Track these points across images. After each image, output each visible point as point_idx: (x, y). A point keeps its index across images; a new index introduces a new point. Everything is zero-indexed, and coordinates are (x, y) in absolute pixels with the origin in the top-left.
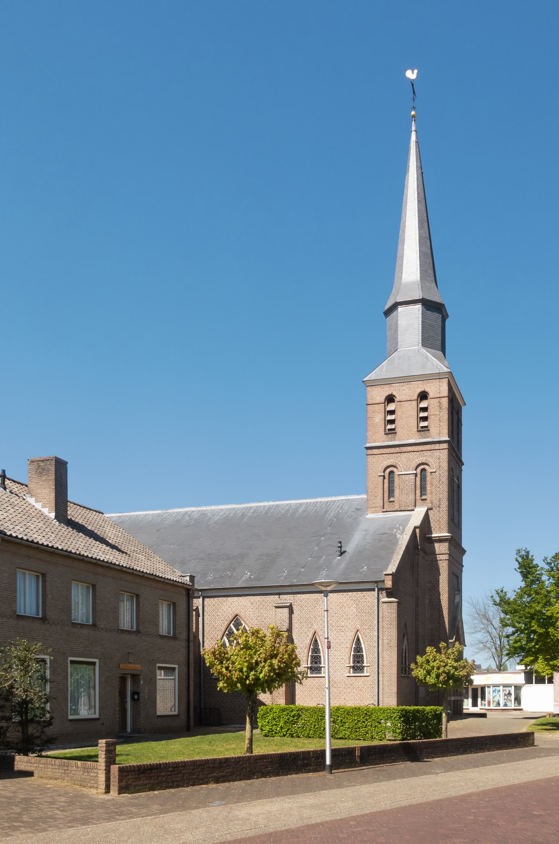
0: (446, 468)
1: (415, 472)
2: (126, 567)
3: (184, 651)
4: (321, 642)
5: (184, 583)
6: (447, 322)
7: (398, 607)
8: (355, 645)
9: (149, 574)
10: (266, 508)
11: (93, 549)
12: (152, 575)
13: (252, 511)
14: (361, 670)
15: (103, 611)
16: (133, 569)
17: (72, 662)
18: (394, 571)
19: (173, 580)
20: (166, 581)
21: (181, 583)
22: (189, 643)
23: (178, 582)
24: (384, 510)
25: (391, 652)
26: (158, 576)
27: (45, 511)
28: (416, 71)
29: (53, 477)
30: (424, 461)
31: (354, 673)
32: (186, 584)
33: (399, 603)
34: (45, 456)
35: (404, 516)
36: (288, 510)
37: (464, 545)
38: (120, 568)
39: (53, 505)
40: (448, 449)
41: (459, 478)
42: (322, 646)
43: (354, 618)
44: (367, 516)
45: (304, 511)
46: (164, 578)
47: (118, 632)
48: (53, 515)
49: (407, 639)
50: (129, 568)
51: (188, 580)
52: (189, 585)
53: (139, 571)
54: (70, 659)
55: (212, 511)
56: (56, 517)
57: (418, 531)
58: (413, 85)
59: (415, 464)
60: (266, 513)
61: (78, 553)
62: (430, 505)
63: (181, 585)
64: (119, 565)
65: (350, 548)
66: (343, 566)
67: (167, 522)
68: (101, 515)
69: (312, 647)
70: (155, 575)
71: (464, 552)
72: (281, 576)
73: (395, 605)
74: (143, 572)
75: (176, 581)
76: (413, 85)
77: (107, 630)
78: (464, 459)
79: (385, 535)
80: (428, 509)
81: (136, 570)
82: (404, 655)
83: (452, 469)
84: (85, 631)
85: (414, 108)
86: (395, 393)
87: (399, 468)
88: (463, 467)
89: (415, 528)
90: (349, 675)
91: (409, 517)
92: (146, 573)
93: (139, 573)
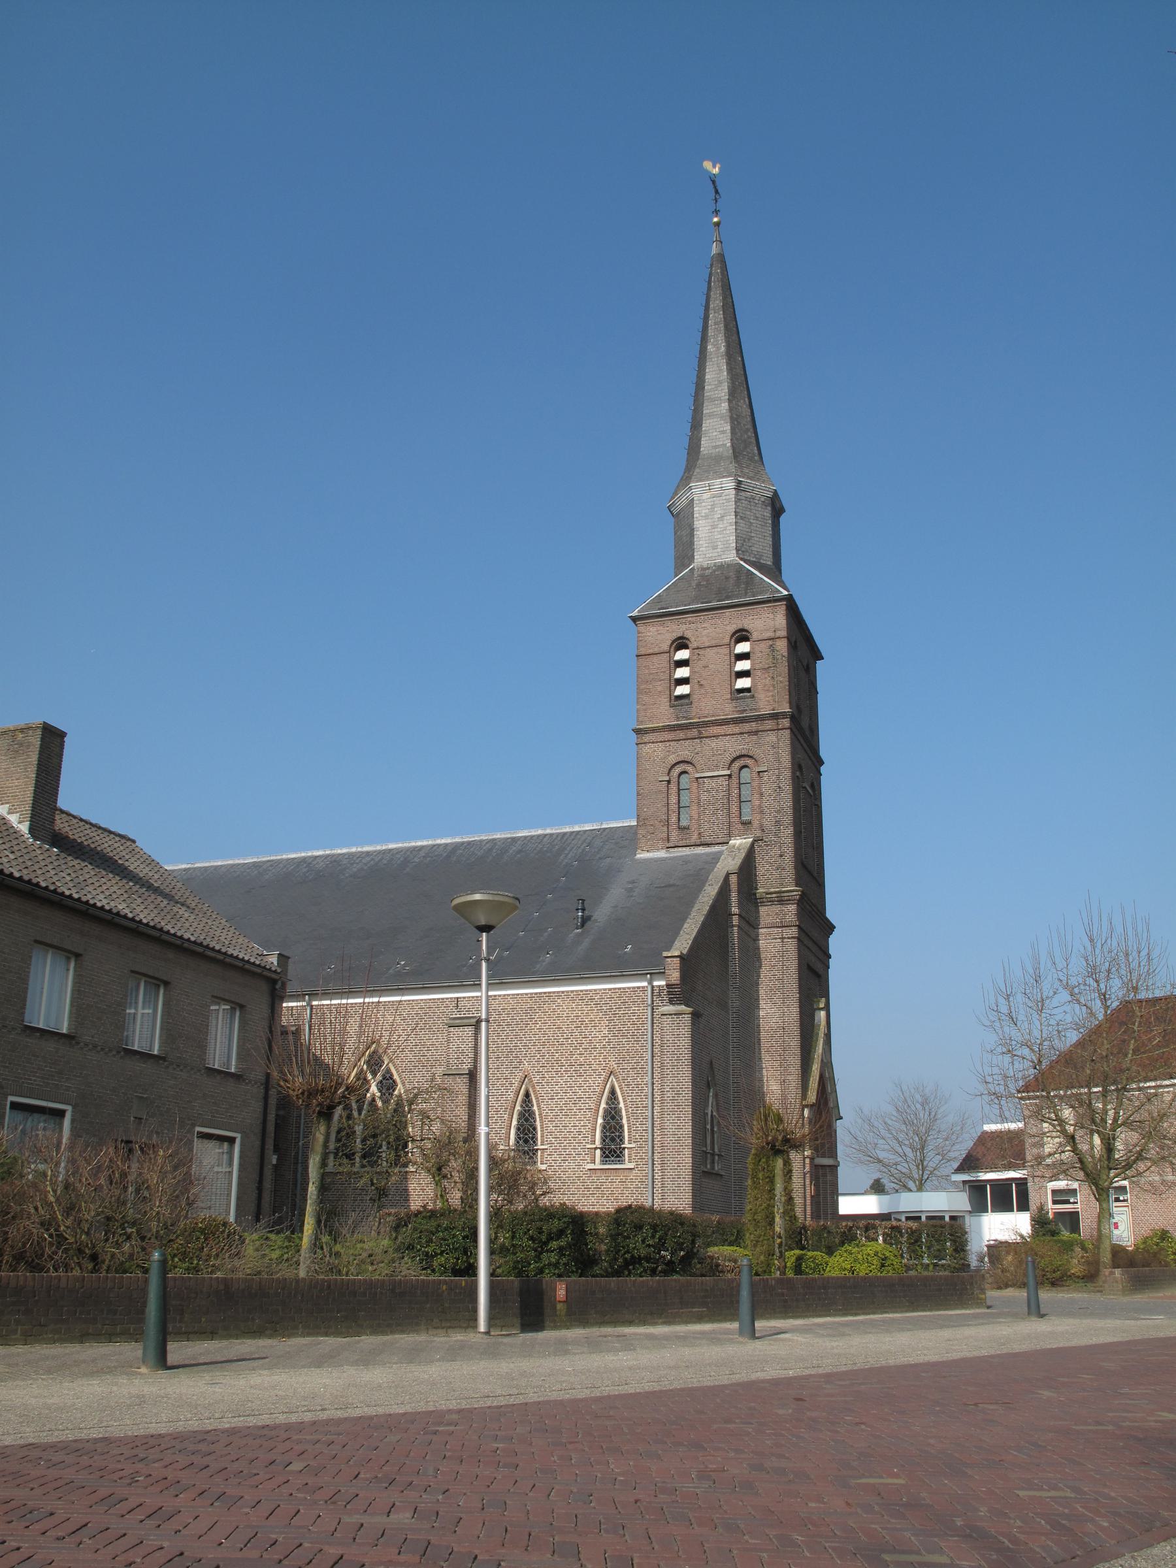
0: (789, 765)
1: (728, 772)
2: (147, 925)
3: (257, 1106)
4: (537, 1099)
5: (264, 967)
6: (783, 519)
7: (693, 1024)
8: (607, 1103)
9: (195, 942)
10: (449, 848)
11: (90, 889)
12: (201, 944)
13: (422, 854)
14: (618, 1156)
15: (97, 1011)
16: (161, 930)
17: (15, 1106)
18: (685, 952)
19: (243, 960)
20: (228, 960)
21: (259, 966)
22: (267, 1090)
23: (254, 964)
24: (671, 844)
25: (679, 1118)
26: (213, 949)
27: (13, 819)
28: (718, 166)
29: (34, 758)
30: (744, 752)
31: (603, 1162)
32: (270, 969)
33: (696, 1016)
34: (21, 723)
35: (707, 854)
36: (490, 850)
37: (830, 914)
38: (134, 925)
39: (28, 807)
40: (791, 729)
41: (816, 787)
42: (539, 1106)
43: (604, 1047)
44: (641, 855)
45: (520, 851)
46: (225, 954)
47: (118, 1052)
48: (24, 828)
49: (716, 1095)
50: (154, 927)
51: (276, 963)
52: (275, 971)
53: (174, 935)
54: (11, 1098)
55: (351, 855)
56: (32, 830)
57: (734, 879)
58: (714, 182)
59: (728, 758)
60: (448, 857)
61: (52, 888)
62: (759, 834)
63: (259, 970)
64: (133, 919)
65: (602, 914)
66: (586, 943)
67: (267, 877)
68: (129, 843)
69: (518, 1108)
70: (207, 947)
71: (831, 928)
72: (464, 966)
73: (688, 1018)
74: (181, 937)
75: (248, 962)
76: (714, 182)
77: (95, 1046)
78: (823, 753)
79: (671, 889)
80: (755, 841)
81: (168, 932)
82: (709, 1127)
83: (800, 767)
84: (50, 1046)
85: (716, 212)
86: (688, 634)
87: (698, 767)
88: (823, 769)
89: (728, 875)
90: (592, 1166)
91: (716, 858)
92: (189, 940)
93: (173, 940)
